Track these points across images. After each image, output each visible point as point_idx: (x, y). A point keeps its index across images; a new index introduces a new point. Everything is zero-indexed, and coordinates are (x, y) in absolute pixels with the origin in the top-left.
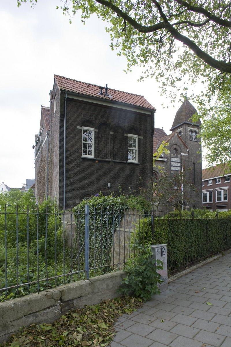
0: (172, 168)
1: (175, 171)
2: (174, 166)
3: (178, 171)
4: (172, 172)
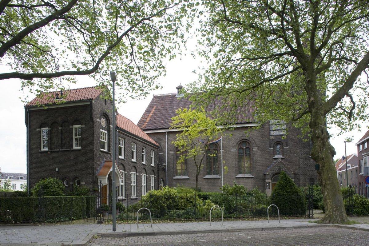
0: (273, 133)
1: (277, 135)
2: (275, 130)
3: (282, 135)
4: (272, 138)
